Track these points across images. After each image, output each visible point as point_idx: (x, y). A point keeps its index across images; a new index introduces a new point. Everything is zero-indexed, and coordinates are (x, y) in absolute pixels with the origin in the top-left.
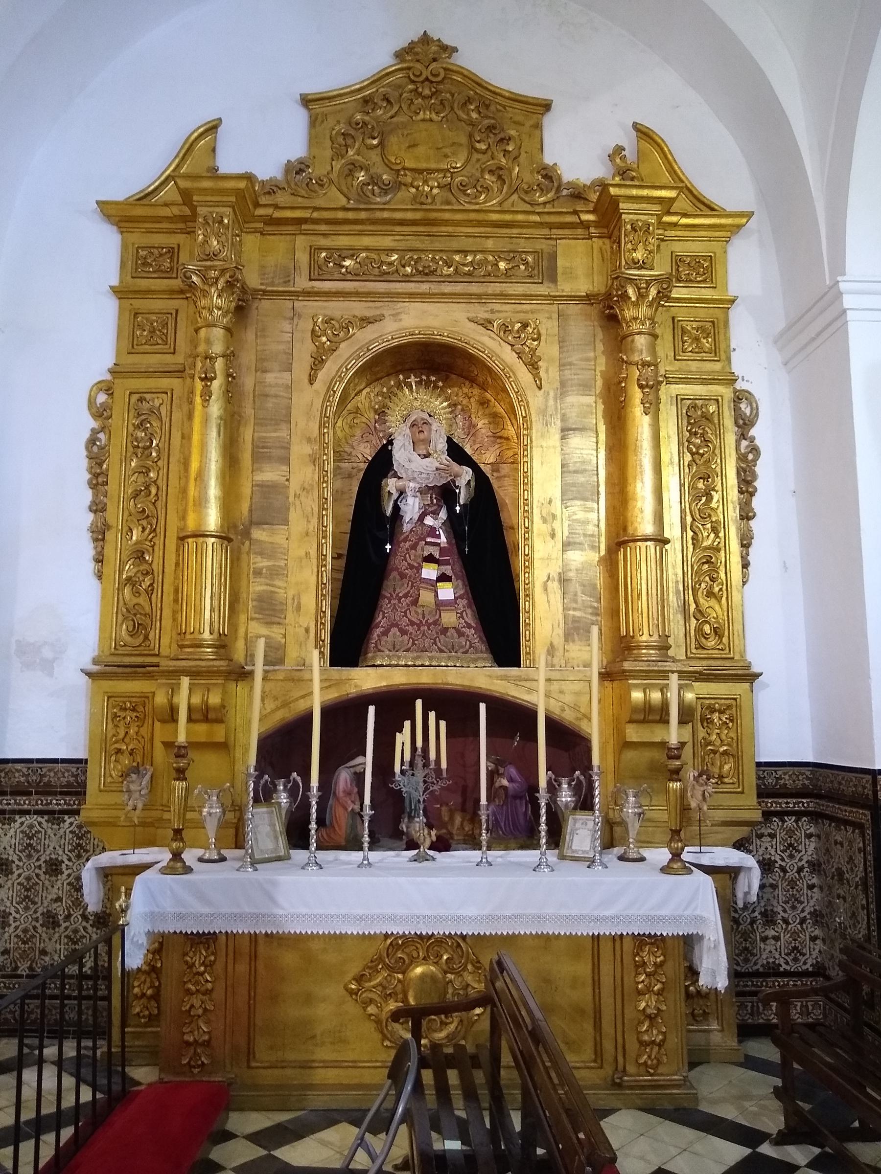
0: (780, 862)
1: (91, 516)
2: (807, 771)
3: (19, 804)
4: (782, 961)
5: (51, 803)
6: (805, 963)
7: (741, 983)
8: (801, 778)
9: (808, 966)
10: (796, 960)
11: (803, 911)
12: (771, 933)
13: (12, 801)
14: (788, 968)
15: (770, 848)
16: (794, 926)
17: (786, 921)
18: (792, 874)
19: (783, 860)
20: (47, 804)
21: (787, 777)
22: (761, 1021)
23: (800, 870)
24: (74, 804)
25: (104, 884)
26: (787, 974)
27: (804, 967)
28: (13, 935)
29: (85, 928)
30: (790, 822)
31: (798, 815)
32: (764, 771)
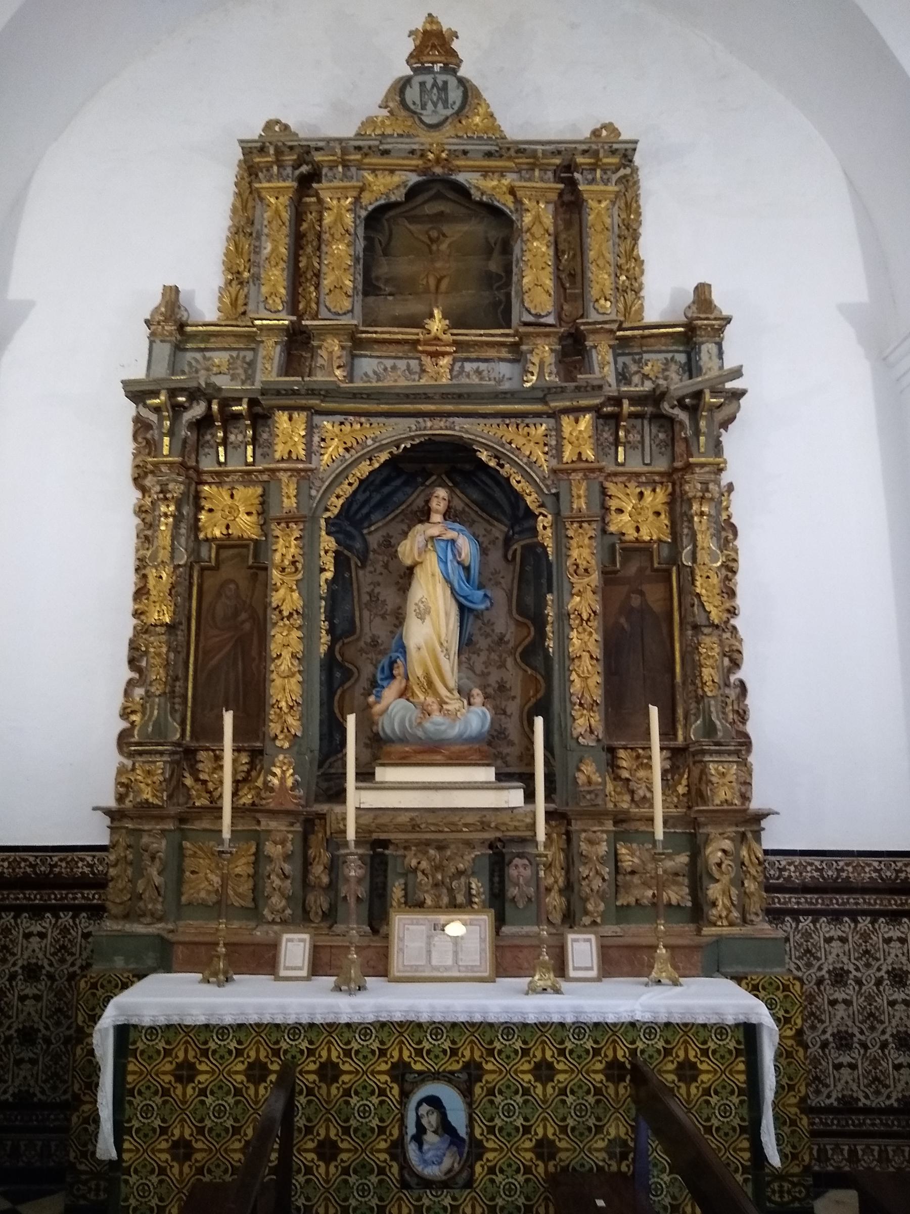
0: (854, 973)
1: (135, 621)
2: (816, 861)
3: (29, 899)
4: (861, 1095)
5: (66, 898)
6: (889, 1097)
7: (52, 1117)
8: (867, 869)
9: (832, 1100)
10: (54, 1088)
11: (824, 1032)
12: (27, 1055)
13: (79, 895)
14: (868, 1103)
15: (841, 955)
16: (874, 1051)
17: (47, 1041)
18: (810, 987)
19: (857, 969)
20: (62, 899)
21: (850, 869)
22: (830, 1168)
23: (820, 982)
24: (876, 903)
25: (132, 983)
26: (867, 1111)
27: (828, 1102)
28: (19, 956)
29: (862, 1032)
30: (864, 923)
31: (875, 915)
32: (37, 857)
